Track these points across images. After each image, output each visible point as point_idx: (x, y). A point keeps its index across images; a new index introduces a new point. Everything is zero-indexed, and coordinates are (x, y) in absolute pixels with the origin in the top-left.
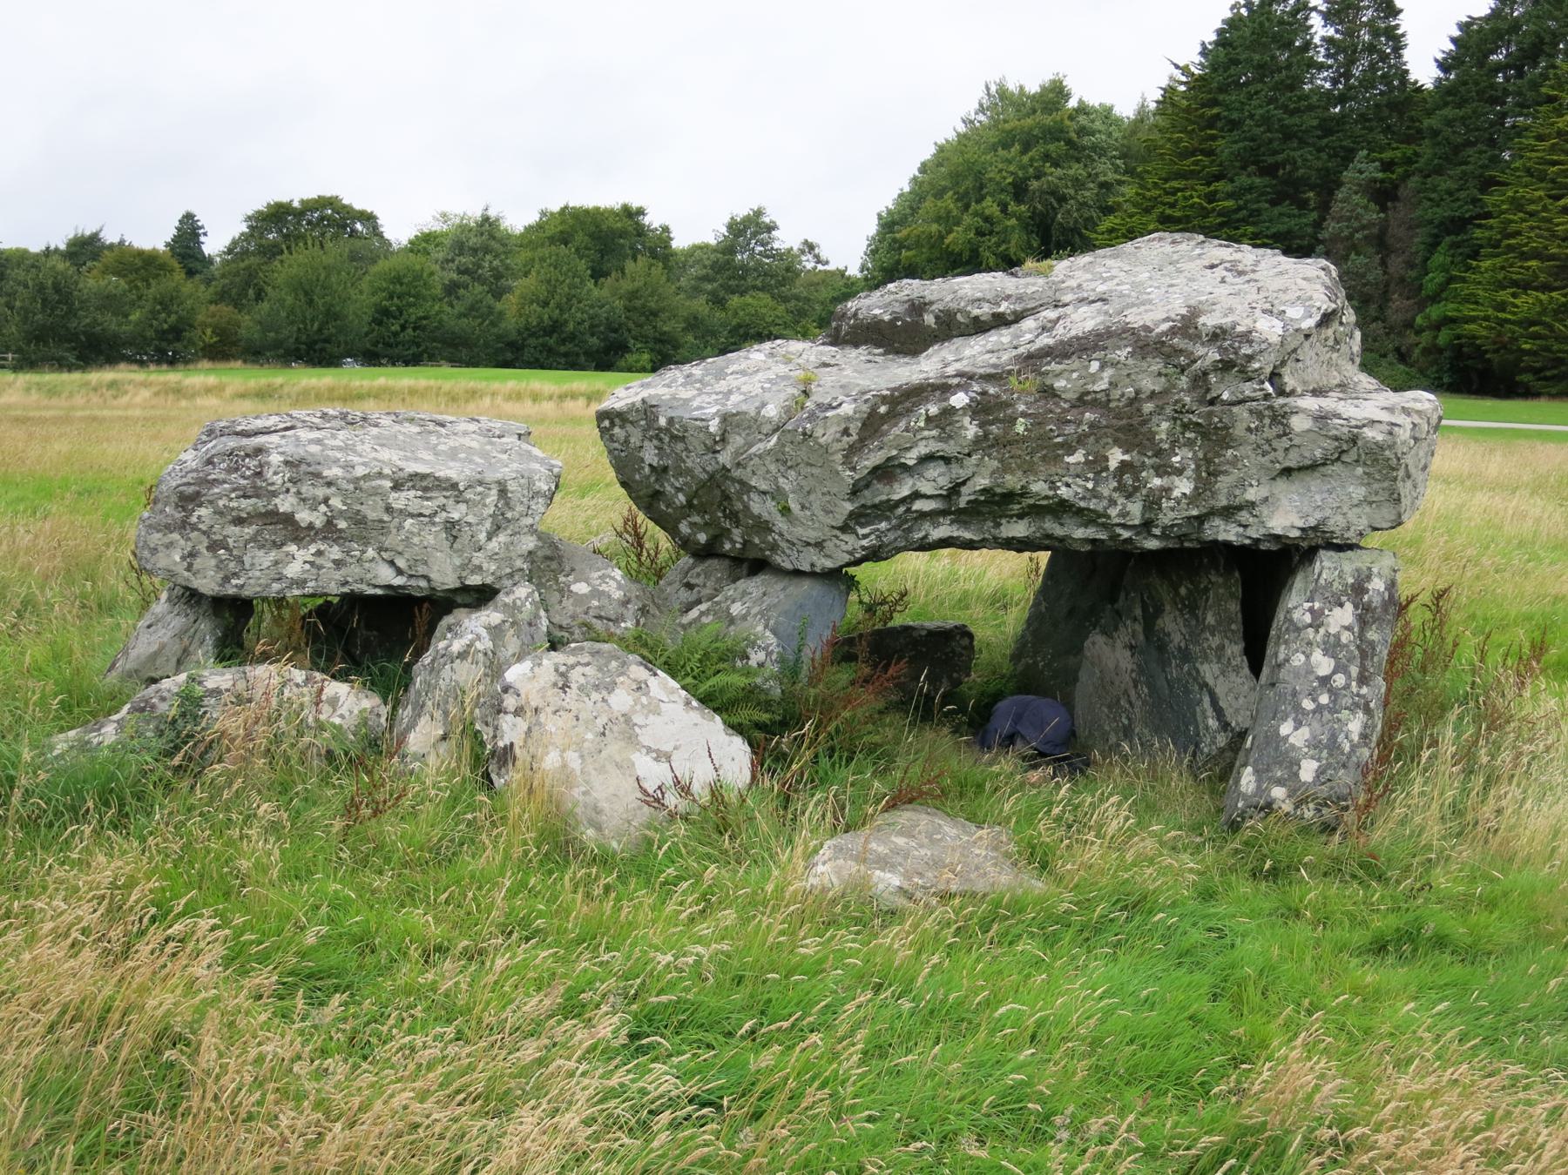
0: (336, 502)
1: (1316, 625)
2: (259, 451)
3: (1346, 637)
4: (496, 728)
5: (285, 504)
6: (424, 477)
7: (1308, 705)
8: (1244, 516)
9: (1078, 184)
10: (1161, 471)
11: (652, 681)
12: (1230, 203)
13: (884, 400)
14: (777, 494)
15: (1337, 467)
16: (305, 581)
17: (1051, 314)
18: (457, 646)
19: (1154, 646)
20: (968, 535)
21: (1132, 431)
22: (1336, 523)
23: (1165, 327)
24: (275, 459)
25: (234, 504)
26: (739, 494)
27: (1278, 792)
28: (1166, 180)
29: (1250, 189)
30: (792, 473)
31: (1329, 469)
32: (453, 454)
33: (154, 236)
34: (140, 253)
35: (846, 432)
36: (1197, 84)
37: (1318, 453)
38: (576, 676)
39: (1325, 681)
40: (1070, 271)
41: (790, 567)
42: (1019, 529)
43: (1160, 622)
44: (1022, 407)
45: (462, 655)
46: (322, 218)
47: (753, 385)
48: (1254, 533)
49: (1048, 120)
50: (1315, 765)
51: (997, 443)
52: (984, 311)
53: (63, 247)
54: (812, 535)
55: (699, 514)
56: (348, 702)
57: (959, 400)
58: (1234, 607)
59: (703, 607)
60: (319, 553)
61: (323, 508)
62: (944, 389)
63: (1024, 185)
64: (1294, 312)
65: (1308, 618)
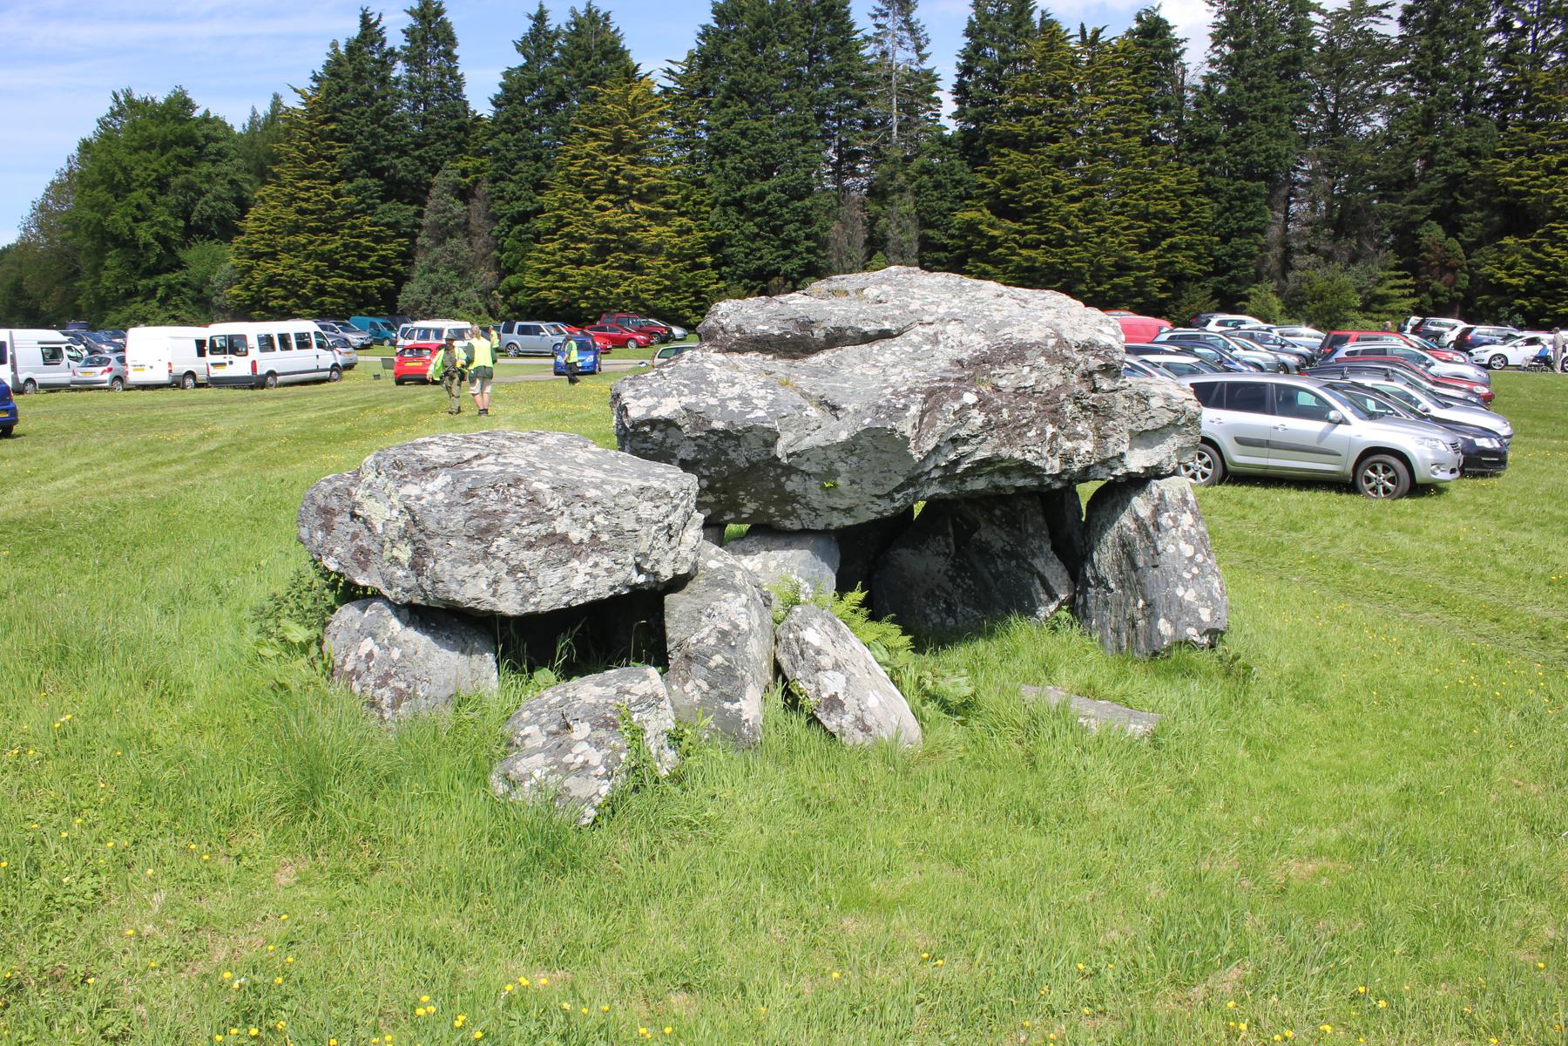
0: (599, 519)
1: (1176, 527)
4: (818, 684)
5: (561, 526)
7: (1187, 576)
9: (209, 178)
12: (352, 199)
16: (585, 591)
25: (524, 531)
29: (365, 188)
39: (1191, 559)
41: (797, 526)
48: (1119, 472)
49: (179, 129)
50: (1208, 611)
52: (870, 328)
58: (1041, 519)
60: (596, 565)
61: (590, 526)
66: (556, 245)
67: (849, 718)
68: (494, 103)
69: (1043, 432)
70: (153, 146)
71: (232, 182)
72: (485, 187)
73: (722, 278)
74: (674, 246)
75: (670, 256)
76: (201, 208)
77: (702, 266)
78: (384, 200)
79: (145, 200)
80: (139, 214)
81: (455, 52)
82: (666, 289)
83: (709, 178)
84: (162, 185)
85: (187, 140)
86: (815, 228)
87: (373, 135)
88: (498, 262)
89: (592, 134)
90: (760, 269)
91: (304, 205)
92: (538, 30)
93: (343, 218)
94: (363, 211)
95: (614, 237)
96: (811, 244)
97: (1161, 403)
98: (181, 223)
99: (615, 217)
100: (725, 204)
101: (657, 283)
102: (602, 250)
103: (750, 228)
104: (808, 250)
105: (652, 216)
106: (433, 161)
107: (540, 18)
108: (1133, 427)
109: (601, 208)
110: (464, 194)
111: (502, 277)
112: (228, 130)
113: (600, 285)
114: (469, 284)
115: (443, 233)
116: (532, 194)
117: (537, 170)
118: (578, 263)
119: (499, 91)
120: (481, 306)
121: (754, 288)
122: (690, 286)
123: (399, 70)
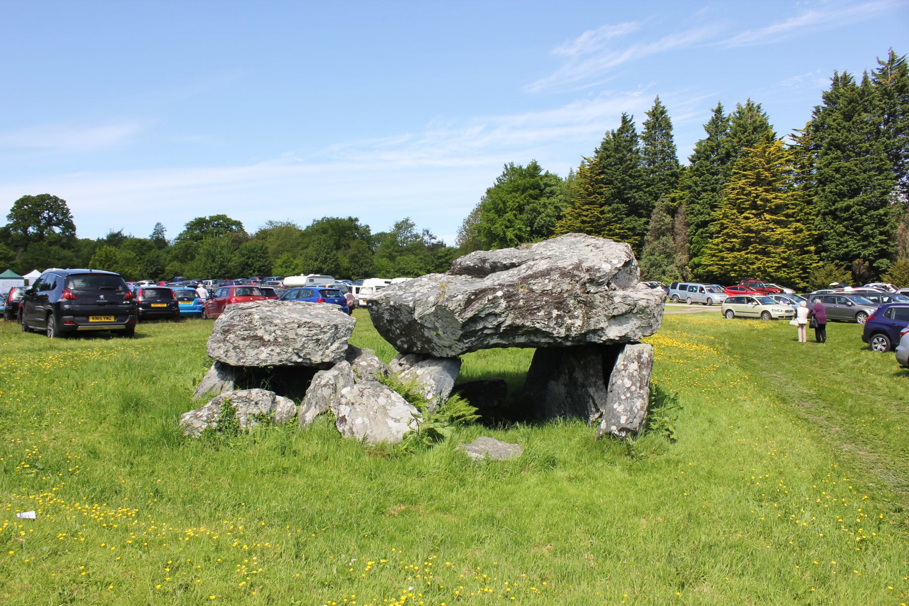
2: (250, 314)
3: (635, 373)
5: (260, 333)
6: (309, 323)
7: (623, 397)
8: (600, 333)
9: (545, 206)
10: (571, 317)
11: (392, 395)
12: (610, 215)
13: (473, 294)
14: (435, 329)
15: (630, 315)
17: (531, 263)
18: (323, 383)
19: (572, 384)
20: (504, 342)
21: (560, 304)
22: (631, 335)
23: (571, 267)
24: (256, 317)
26: (420, 329)
27: (614, 428)
28: (583, 205)
29: (618, 209)
30: (440, 321)
31: (628, 316)
32: (316, 316)
33: (144, 233)
34: (139, 241)
35: (460, 305)
36: (593, 166)
37: (624, 310)
38: (366, 392)
39: (628, 389)
40: (539, 247)
42: (522, 340)
43: (574, 375)
44: (521, 296)
45: (325, 386)
46: (218, 224)
47: (424, 290)
48: (604, 338)
49: (532, 181)
51: (514, 308)
53: (105, 238)
54: (447, 343)
55: (406, 336)
56: (284, 404)
57: (500, 294)
58: (600, 367)
59: (406, 372)
60: (272, 350)
62: (494, 290)
63: (521, 207)
64: (615, 262)
65: (622, 367)
66: (720, 240)
67: (347, 427)
68: (691, 160)
69: (550, 313)
70: (518, 190)
71: (556, 207)
72: (684, 208)
73: (822, 259)
74: (789, 241)
75: (787, 246)
76: (540, 221)
77: (808, 252)
78: (628, 215)
79: (512, 217)
80: (508, 224)
81: (672, 133)
82: (784, 266)
83: (815, 199)
84: (521, 209)
85: (536, 186)
86: (887, 228)
87: (623, 180)
88: (689, 249)
89: (744, 176)
90: (846, 254)
91: (585, 218)
92: (717, 118)
93: (605, 225)
94: (616, 222)
95: (753, 235)
96: (883, 237)
97: (620, 300)
98: (529, 229)
99: (754, 223)
100: (825, 214)
101: (778, 263)
102: (746, 243)
103: (840, 228)
104: (881, 242)
105: (777, 222)
106: (656, 193)
107: (719, 111)
108: (606, 313)
109: (746, 218)
110: (673, 212)
111: (691, 258)
112: (558, 180)
113: (743, 264)
114: (672, 262)
115: (659, 233)
116: (709, 210)
117: (713, 197)
118: (732, 250)
119: (694, 153)
120: (679, 275)
121: (842, 265)
122: (800, 264)
123: (641, 144)
